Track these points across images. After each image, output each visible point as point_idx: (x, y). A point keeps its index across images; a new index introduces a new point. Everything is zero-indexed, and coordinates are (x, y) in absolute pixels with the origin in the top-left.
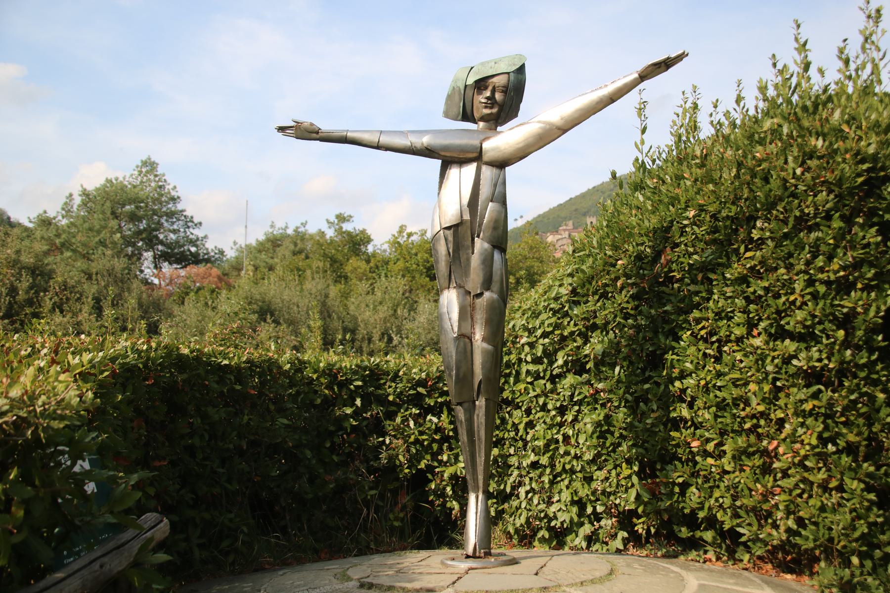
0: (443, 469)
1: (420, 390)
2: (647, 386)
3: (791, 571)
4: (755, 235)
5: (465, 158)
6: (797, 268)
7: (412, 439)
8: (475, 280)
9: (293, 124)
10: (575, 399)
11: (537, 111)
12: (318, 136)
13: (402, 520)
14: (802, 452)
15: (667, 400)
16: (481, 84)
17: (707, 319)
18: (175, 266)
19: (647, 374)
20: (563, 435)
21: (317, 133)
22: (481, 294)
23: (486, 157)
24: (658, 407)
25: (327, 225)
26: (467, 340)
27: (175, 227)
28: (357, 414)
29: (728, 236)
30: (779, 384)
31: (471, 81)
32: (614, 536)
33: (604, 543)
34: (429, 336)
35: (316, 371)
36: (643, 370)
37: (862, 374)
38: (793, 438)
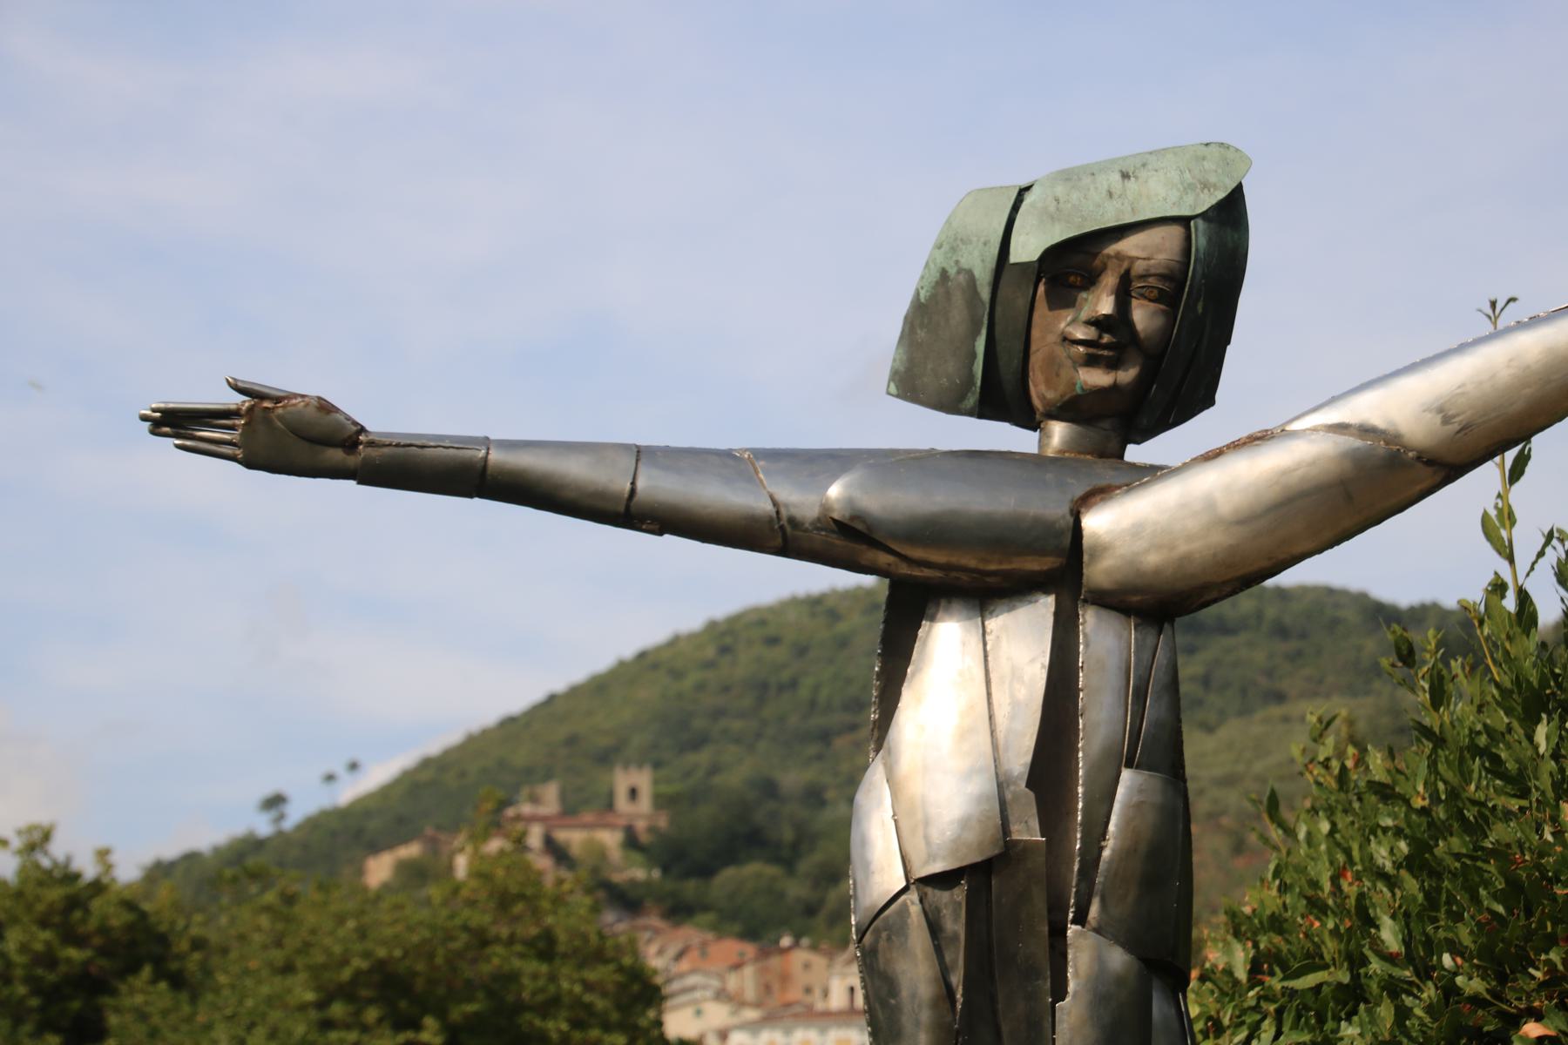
5: (1006, 575)
9: (235, 400)
12: (352, 461)
16: (1071, 264)
23: (1098, 572)
31: (1027, 249)
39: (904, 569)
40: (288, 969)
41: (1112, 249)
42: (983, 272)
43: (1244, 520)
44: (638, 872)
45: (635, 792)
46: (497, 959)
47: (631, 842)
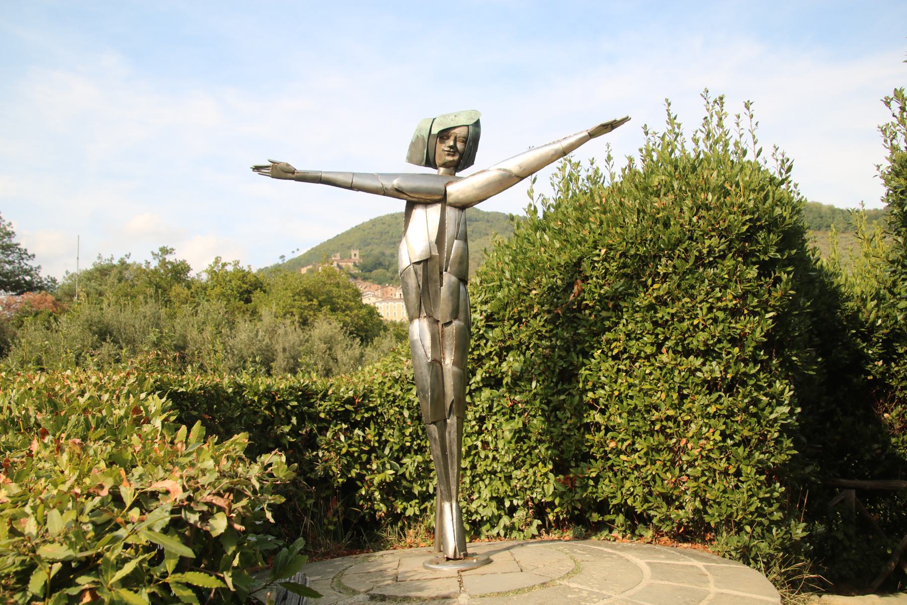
0: (372, 476)
1: (348, 407)
2: (562, 397)
3: (686, 541)
4: (661, 270)
6: (699, 298)
7: (344, 451)
8: (443, 310)
9: (269, 164)
10: (494, 410)
11: (488, 163)
12: (293, 176)
13: (335, 524)
14: (708, 447)
15: (581, 409)
16: (444, 135)
17: (619, 340)
18: (11, 293)
19: (559, 387)
20: (482, 441)
21: (293, 173)
22: (450, 322)
23: (450, 199)
24: (572, 415)
25: (152, 257)
26: (438, 364)
27: (10, 258)
28: (294, 432)
29: (637, 269)
30: (685, 392)
31: (435, 131)
32: (529, 524)
33: (519, 530)
34: (250, 351)
35: (256, 394)
36: (556, 384)
37: (752, 382)
38: (699, 436)
39: (410, 199)
40: (286, 289)
41: (453, 131)
42: (426, 136)
43: (480, 188)
44: (356, 271)
45: (356, 255)
46: (327, 288)
47: (355, 265)
